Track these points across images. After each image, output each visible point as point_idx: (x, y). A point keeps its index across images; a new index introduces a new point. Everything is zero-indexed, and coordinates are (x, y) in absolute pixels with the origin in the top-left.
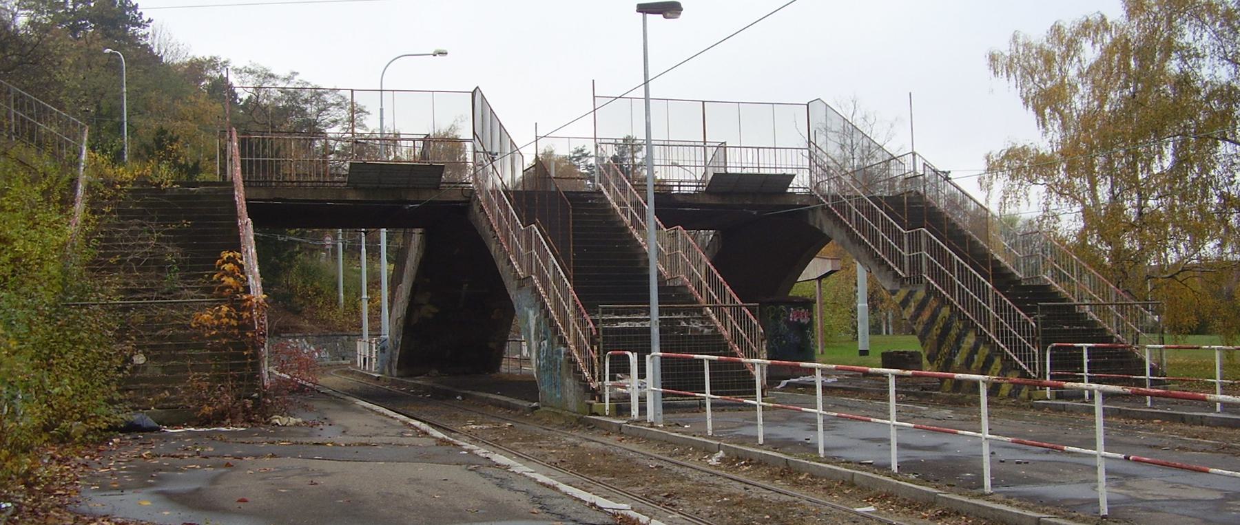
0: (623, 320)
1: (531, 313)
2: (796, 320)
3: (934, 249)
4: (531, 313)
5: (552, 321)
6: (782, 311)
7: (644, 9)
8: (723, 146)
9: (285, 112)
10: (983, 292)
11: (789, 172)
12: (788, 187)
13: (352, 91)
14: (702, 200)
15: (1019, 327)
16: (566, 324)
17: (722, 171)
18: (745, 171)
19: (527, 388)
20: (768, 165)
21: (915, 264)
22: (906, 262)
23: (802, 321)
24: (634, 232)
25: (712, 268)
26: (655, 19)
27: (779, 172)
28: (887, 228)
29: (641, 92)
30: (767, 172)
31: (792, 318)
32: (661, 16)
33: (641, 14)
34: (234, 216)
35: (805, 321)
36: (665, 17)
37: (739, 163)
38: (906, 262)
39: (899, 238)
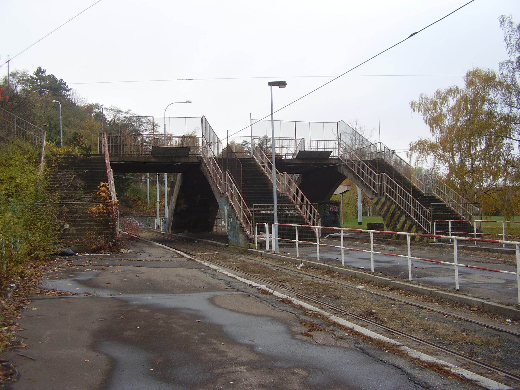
0: (263, 210)
1: (225, 207)
2: (332, 210)
3: (388, 181)
4: (225, 207)
5: (234, 211)
6: (327, 206)
7: (271, 84)
8: (303, 140)
9: (126, 126)
10: (408, 199)
11: (330, 150)
12: (329, 156)
13: (153, 117)
14: (294, 162)
15: (423, 213)
16: (239, 212)
17: (303, 150)
18: (312, 150)
19: (224, 238)
20: (321, 147)
21: (381, 187)
22: (377, 186)
23: (335, 211)
24: (267, 174)
25: (299, 189)
26: (275, 88)
27: (326, 150)
28: (370, 173)
29: (270, 118)
30: (321, 150)
32: (278, 87)
33: (270, 86)
34: (105, 168)
35: (336, 210)
36: (280, 87)
37: (309, 147)
38: (377, 186)
39: (374, 177)
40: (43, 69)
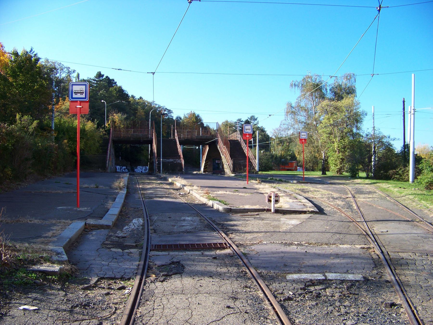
31: (217, 162)
35: (219, 162)
40: (102, 73)
